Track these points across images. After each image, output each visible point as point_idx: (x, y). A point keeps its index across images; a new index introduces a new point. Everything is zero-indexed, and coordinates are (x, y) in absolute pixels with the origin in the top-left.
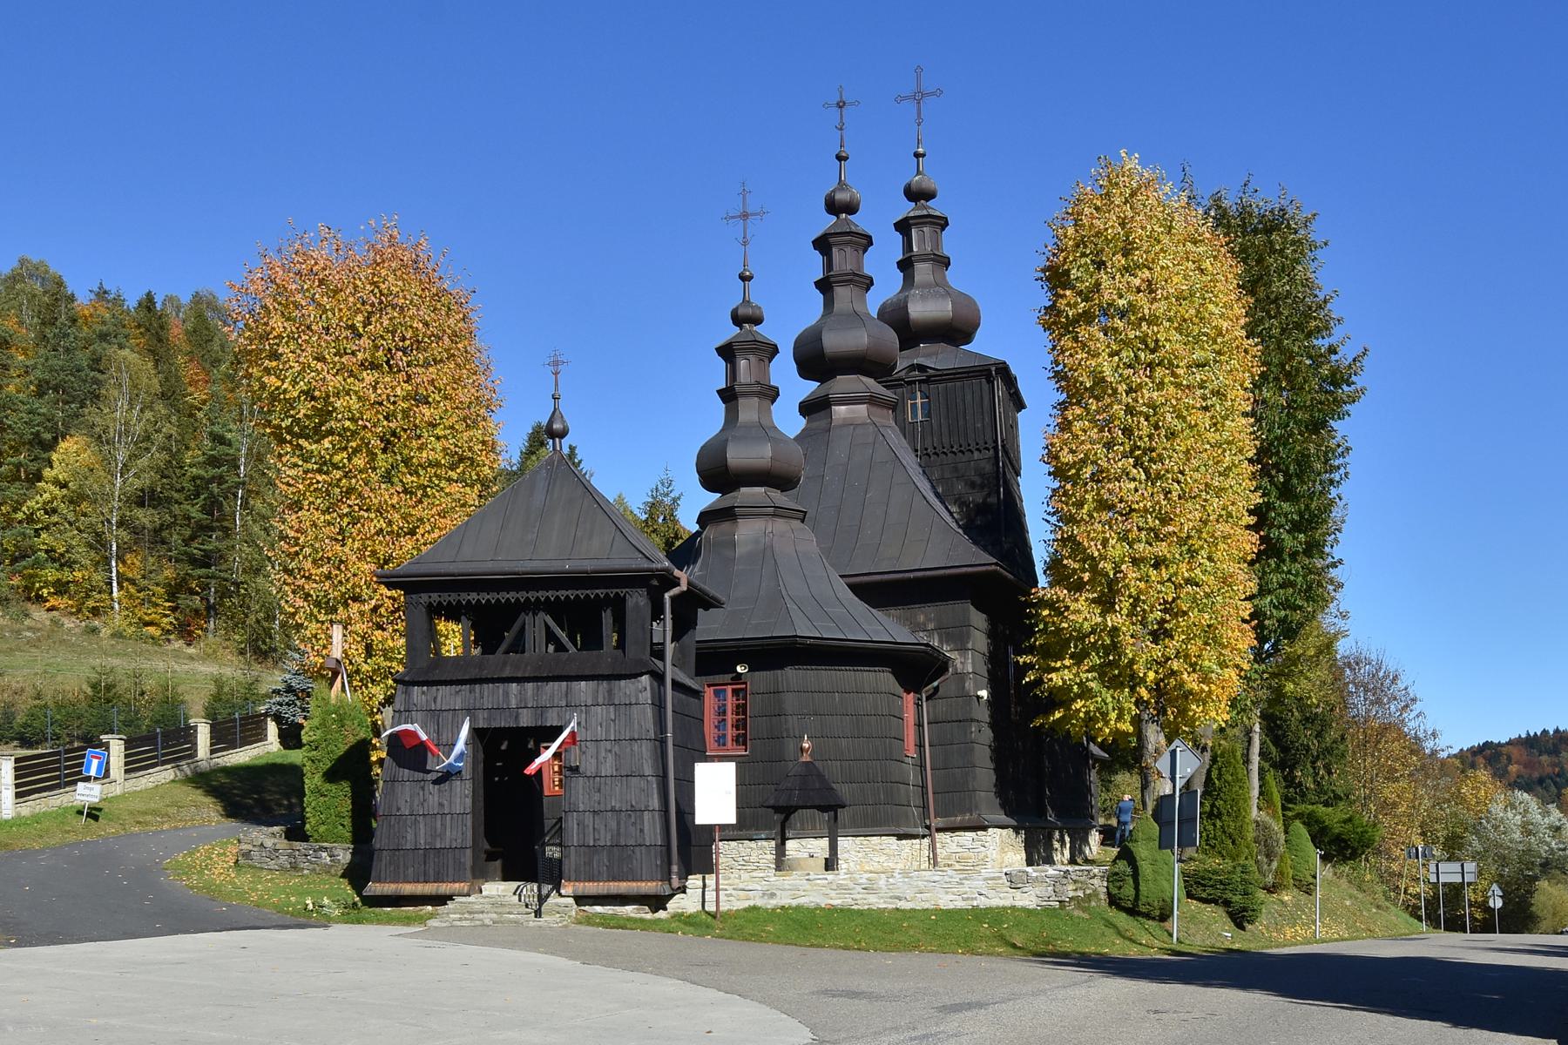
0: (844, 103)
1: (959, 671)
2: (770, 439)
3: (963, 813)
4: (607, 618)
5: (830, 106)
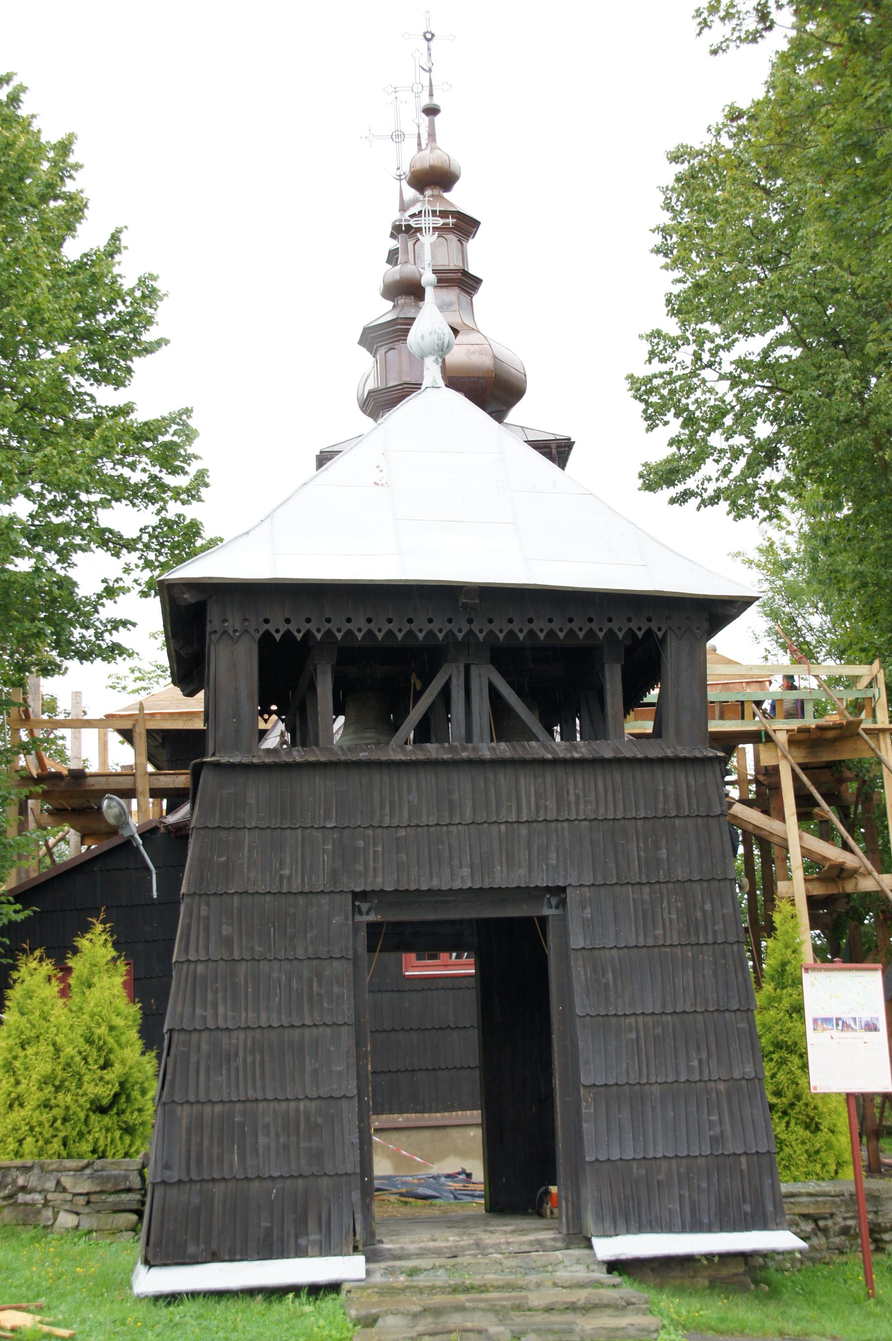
0: (433, 35)
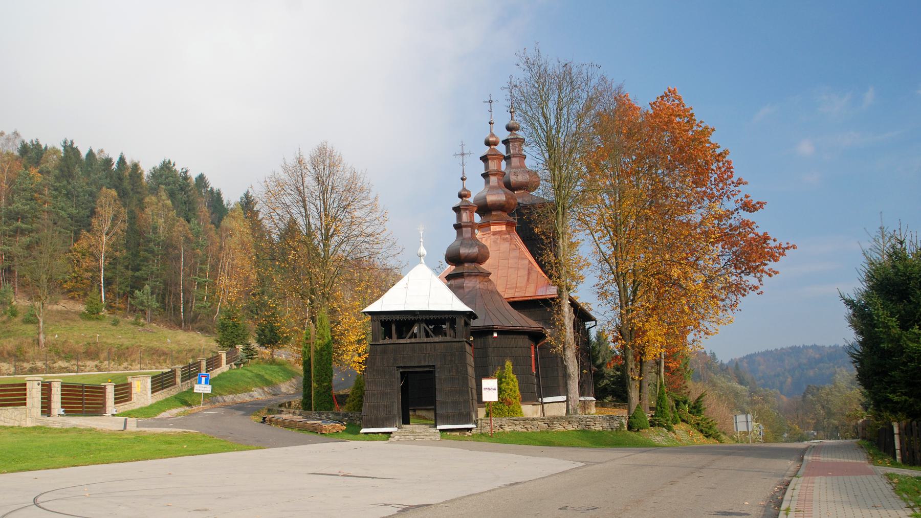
0: (492, 101)
2: (477, 245)
4: (81, 308)
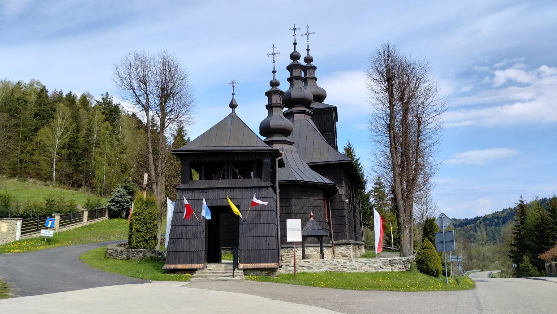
0: (296, 29)
1: (340, 193)
3: (342, 239)
5: (291, 29)
